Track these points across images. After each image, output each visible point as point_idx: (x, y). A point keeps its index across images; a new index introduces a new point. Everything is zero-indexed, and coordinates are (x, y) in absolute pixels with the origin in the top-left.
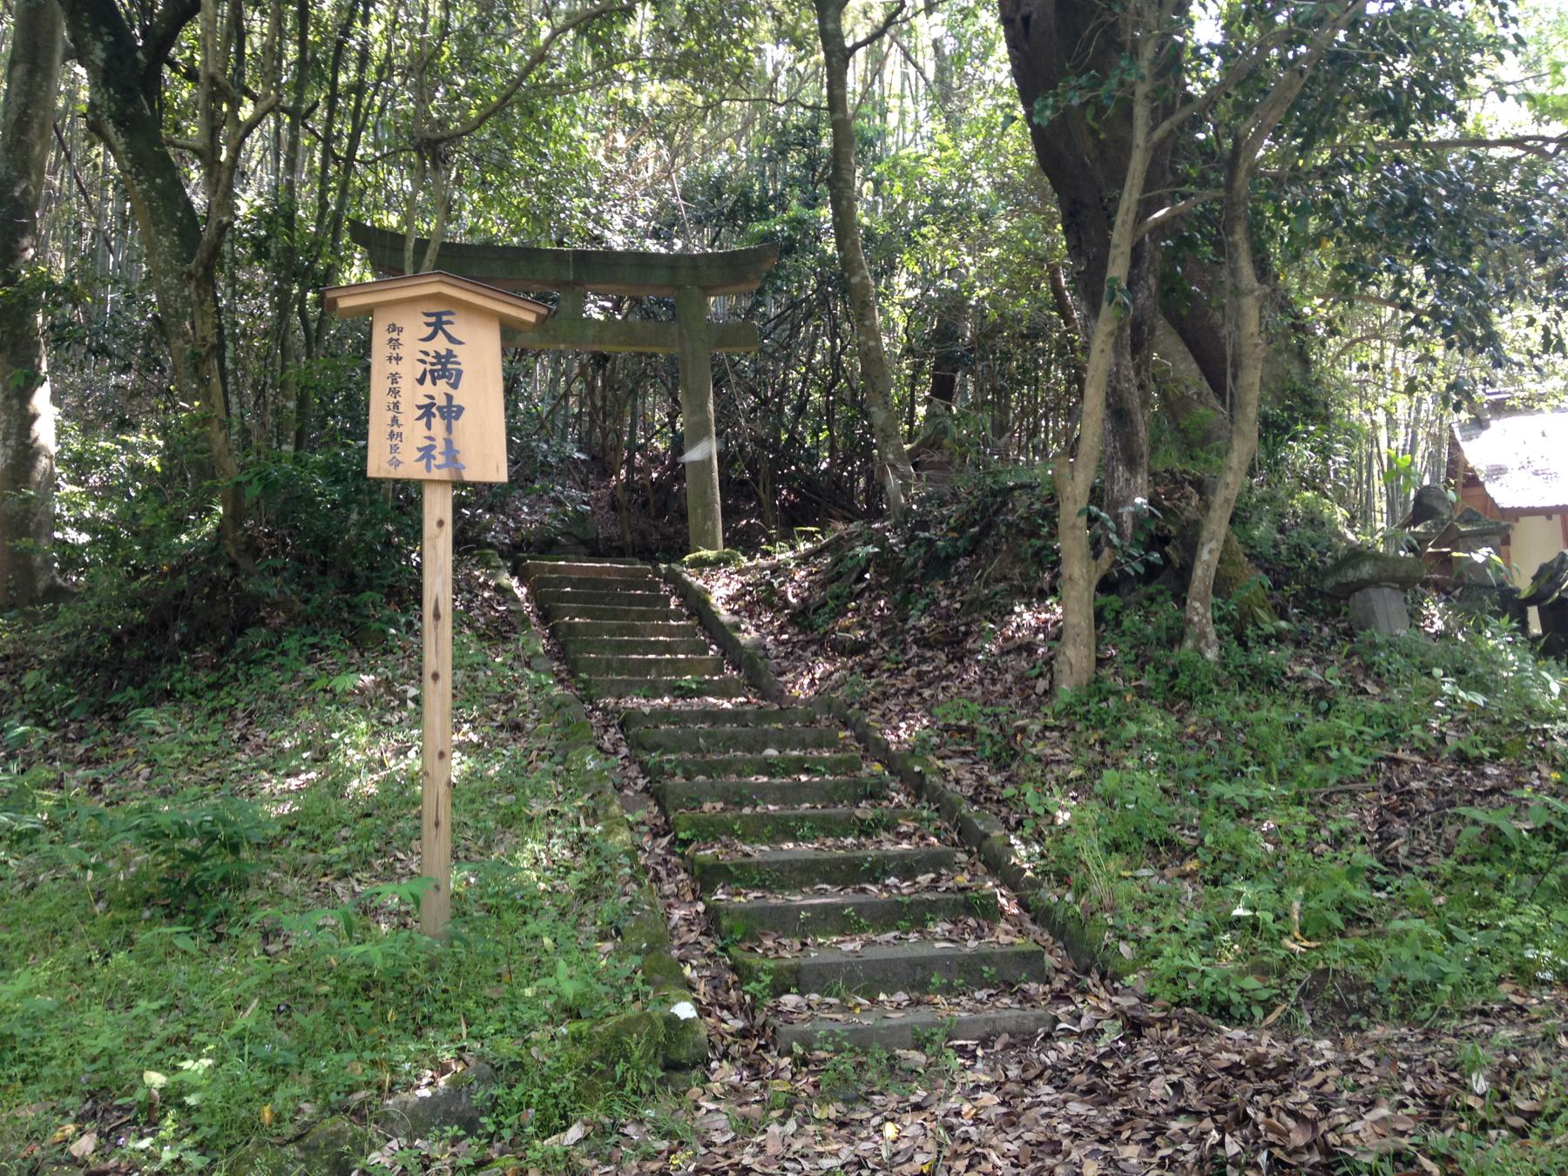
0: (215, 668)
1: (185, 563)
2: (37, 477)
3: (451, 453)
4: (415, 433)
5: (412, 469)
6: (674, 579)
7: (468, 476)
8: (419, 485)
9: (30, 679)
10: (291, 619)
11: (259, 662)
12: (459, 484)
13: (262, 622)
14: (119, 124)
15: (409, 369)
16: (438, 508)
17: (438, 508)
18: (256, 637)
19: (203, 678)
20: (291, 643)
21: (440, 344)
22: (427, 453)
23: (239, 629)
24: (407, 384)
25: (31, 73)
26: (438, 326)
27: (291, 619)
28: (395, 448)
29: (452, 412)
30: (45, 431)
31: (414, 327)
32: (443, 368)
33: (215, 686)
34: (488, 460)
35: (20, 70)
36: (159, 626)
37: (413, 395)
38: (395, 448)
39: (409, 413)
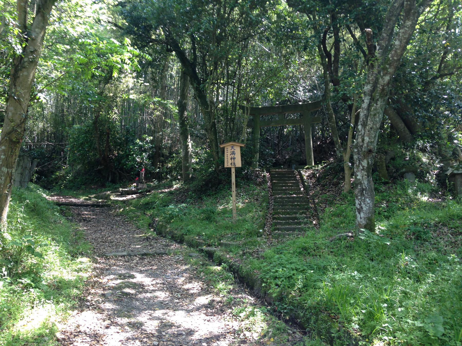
0: (216, 191)
1: (211, 173)
2: (189, 155)
3: (234, 163)
4: (230, 161)
5: (230, 166)
6: (299, 172)
7: (237, 166)
8: (231, 168)
9: (190, 193)
10: (227, 183)
11: (221, 190)
12: (236, 168)
13: (222, 183)
14: (199, 97)
15: (229, 154)
16: (233, 170)
17: (233, 170)
18: (221, 186)
19: (214, 193)
20: (226, 187)
21: (233, 150)
22: (231, 164)
23: (219, 184)
24: (229, 155)
25: (184, 80)
26: (232, 148)
27: (227, 183)
28: (227, 164)
29: (234, 158)
30: (190, 149)
31: (230, 148)
32: (233, 153)
33: (215, 194)
34: (239, 164)
35: (182, 80)
36: (207, 185)
37: (230, 157)
38: (227, 164)
39: (229, 159)
